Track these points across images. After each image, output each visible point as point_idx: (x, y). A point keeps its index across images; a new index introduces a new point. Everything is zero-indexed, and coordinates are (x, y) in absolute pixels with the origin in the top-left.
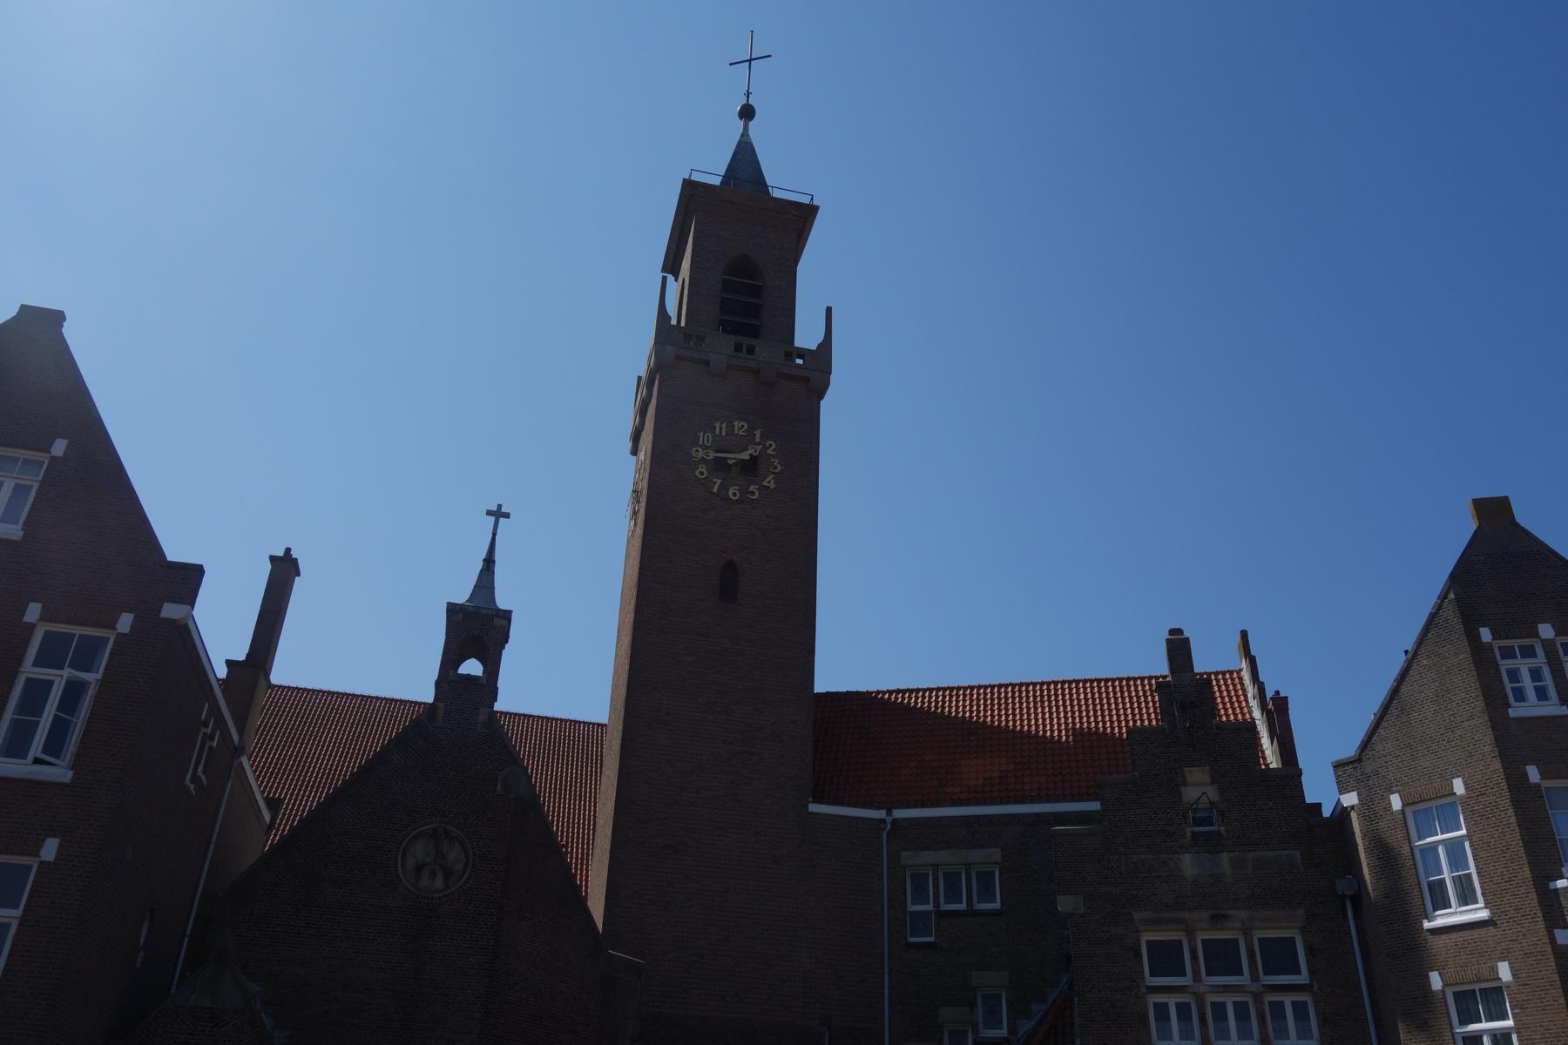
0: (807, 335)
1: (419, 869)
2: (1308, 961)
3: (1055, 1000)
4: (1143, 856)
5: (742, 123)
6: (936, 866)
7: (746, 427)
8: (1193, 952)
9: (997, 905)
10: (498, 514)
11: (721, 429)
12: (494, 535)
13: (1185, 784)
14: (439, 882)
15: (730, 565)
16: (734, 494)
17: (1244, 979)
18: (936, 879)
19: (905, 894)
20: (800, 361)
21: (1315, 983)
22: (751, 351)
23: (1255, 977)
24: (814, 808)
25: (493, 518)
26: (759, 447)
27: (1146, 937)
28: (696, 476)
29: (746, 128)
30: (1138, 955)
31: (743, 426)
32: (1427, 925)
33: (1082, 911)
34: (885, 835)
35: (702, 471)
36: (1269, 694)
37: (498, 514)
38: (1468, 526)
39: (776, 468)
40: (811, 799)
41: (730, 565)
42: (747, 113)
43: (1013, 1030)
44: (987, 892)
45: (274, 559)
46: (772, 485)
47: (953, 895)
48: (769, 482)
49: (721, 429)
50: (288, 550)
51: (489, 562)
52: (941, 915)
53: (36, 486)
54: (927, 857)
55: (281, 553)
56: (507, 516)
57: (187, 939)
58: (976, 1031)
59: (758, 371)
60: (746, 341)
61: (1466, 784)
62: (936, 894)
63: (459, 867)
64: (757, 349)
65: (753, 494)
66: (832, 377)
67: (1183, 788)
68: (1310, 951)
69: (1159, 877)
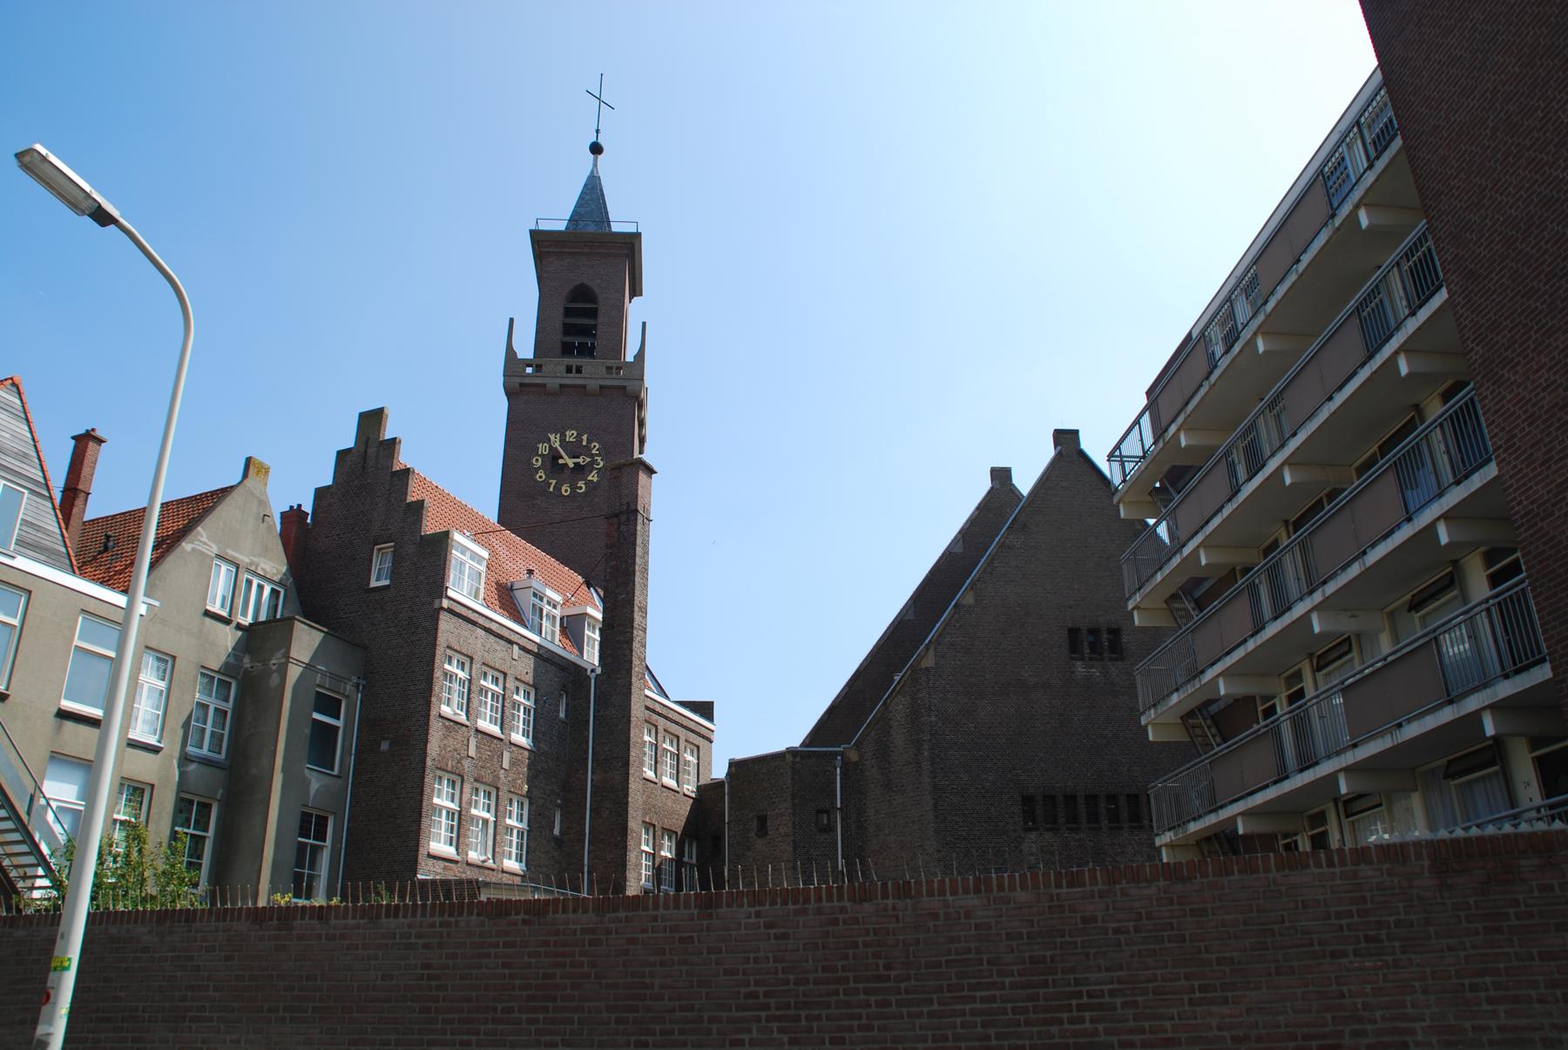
5: (112, 227)
16: (566, 491)
20: (529, 370)
22: (579, 370)
26: (588, 460)
29: (595, 164)
35: (541, 476)
50: (73, 438)
65: (581, 488)
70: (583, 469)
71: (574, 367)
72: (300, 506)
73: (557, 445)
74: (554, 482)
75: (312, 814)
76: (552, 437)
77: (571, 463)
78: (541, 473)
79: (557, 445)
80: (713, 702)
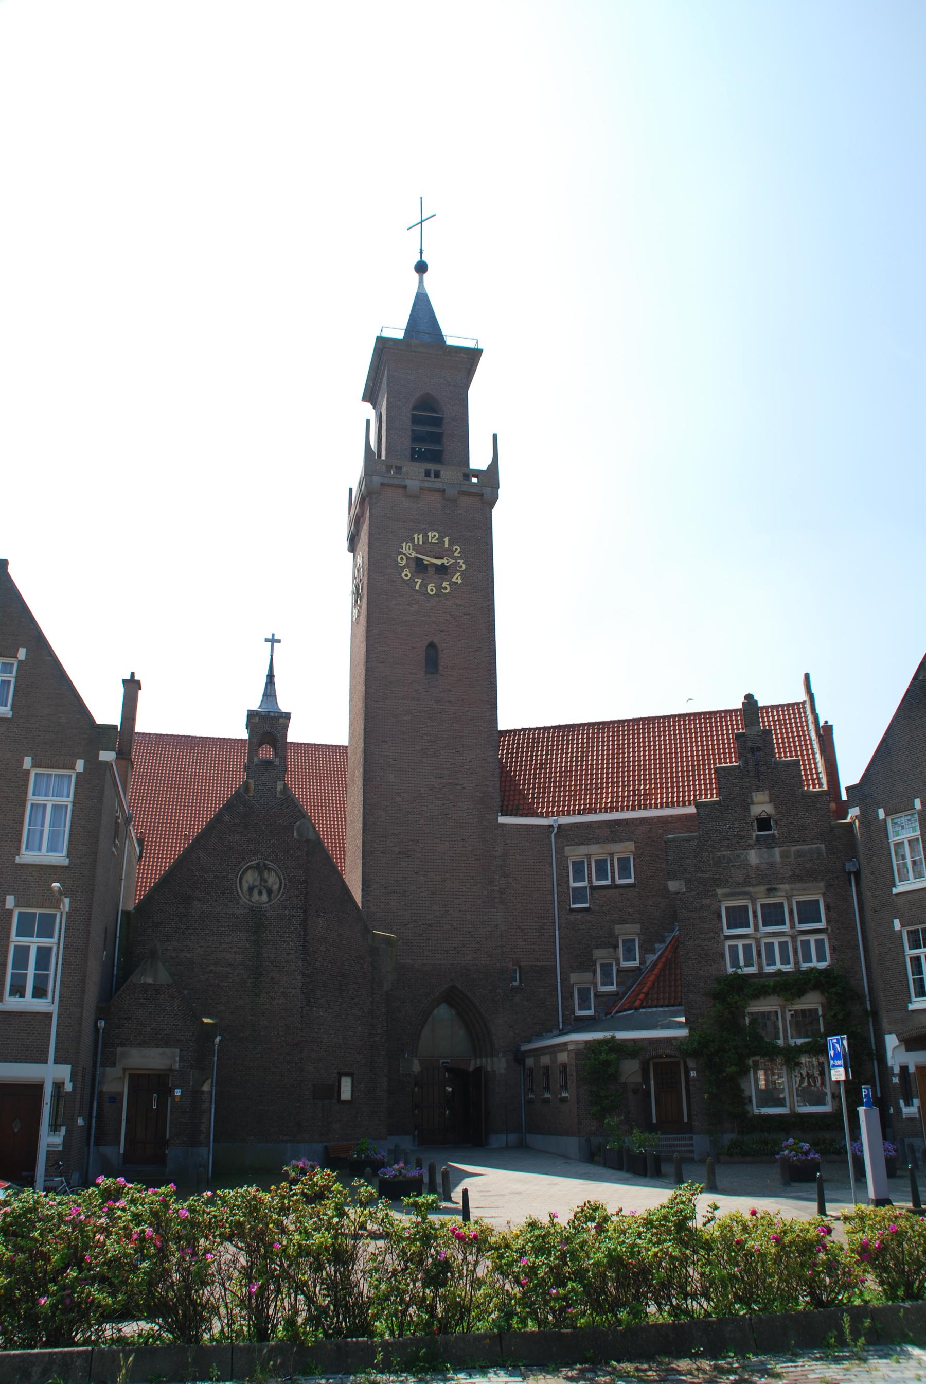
0: (479, 460)
1: (251, 889)
2: (826, 915)
3: (671, 941)
4: (724, 853)
6: (589, 856)
7: (437, 536)
8: (755, 913)
9: (631, 881)
10: (273, 641)
11: (418, 539)
12: (272, 656)
13: (753, 803)
14: (265, 897)
15: (432, 646)
16: (432, 590)
17: (785, 928)
19: (568, 876)
20: (475, 480)
21: (829, 928)
22: (437, 475)
23: (793, 926)
24: (502, 820)
25: (270, 643)
26: (452, 561)
28: (402, 578)
29: (421, 281)
30: (719, 916)
31: (435, 536)
32: (895, 891)
33: (684, 890)
34: (553, 836)
35: (406, 574)
36: (821, 723)
37: (273, 641)
39: (462, 567)
40: (500, 814)
41: (432, 646)
42: (421, 268)
43: (643, 961)
45: (125, 682)
46: (459, 581)
48: (457, 578)
49: (418, 539)
50: (133, 674)
51: (271, 677)
52: (593, 888)
53: (13, 680)
54: (583, 850)
55: (128, 677)
56: (279, 641)
57: (118, 939)
58: (618, 964)
59: (444, 491)
60: (433, 467)
63: (276, 887)
64: (442, 473)
65: (446, 589)
66: (500, 491)
67: (751, 806)
68: (828, 908)
69: (735, 865)
70: (446, 570)
71: (432, 472)
74: (420, 581)
75: (918, 930)
78: (406, 572)
80: (289, 714)
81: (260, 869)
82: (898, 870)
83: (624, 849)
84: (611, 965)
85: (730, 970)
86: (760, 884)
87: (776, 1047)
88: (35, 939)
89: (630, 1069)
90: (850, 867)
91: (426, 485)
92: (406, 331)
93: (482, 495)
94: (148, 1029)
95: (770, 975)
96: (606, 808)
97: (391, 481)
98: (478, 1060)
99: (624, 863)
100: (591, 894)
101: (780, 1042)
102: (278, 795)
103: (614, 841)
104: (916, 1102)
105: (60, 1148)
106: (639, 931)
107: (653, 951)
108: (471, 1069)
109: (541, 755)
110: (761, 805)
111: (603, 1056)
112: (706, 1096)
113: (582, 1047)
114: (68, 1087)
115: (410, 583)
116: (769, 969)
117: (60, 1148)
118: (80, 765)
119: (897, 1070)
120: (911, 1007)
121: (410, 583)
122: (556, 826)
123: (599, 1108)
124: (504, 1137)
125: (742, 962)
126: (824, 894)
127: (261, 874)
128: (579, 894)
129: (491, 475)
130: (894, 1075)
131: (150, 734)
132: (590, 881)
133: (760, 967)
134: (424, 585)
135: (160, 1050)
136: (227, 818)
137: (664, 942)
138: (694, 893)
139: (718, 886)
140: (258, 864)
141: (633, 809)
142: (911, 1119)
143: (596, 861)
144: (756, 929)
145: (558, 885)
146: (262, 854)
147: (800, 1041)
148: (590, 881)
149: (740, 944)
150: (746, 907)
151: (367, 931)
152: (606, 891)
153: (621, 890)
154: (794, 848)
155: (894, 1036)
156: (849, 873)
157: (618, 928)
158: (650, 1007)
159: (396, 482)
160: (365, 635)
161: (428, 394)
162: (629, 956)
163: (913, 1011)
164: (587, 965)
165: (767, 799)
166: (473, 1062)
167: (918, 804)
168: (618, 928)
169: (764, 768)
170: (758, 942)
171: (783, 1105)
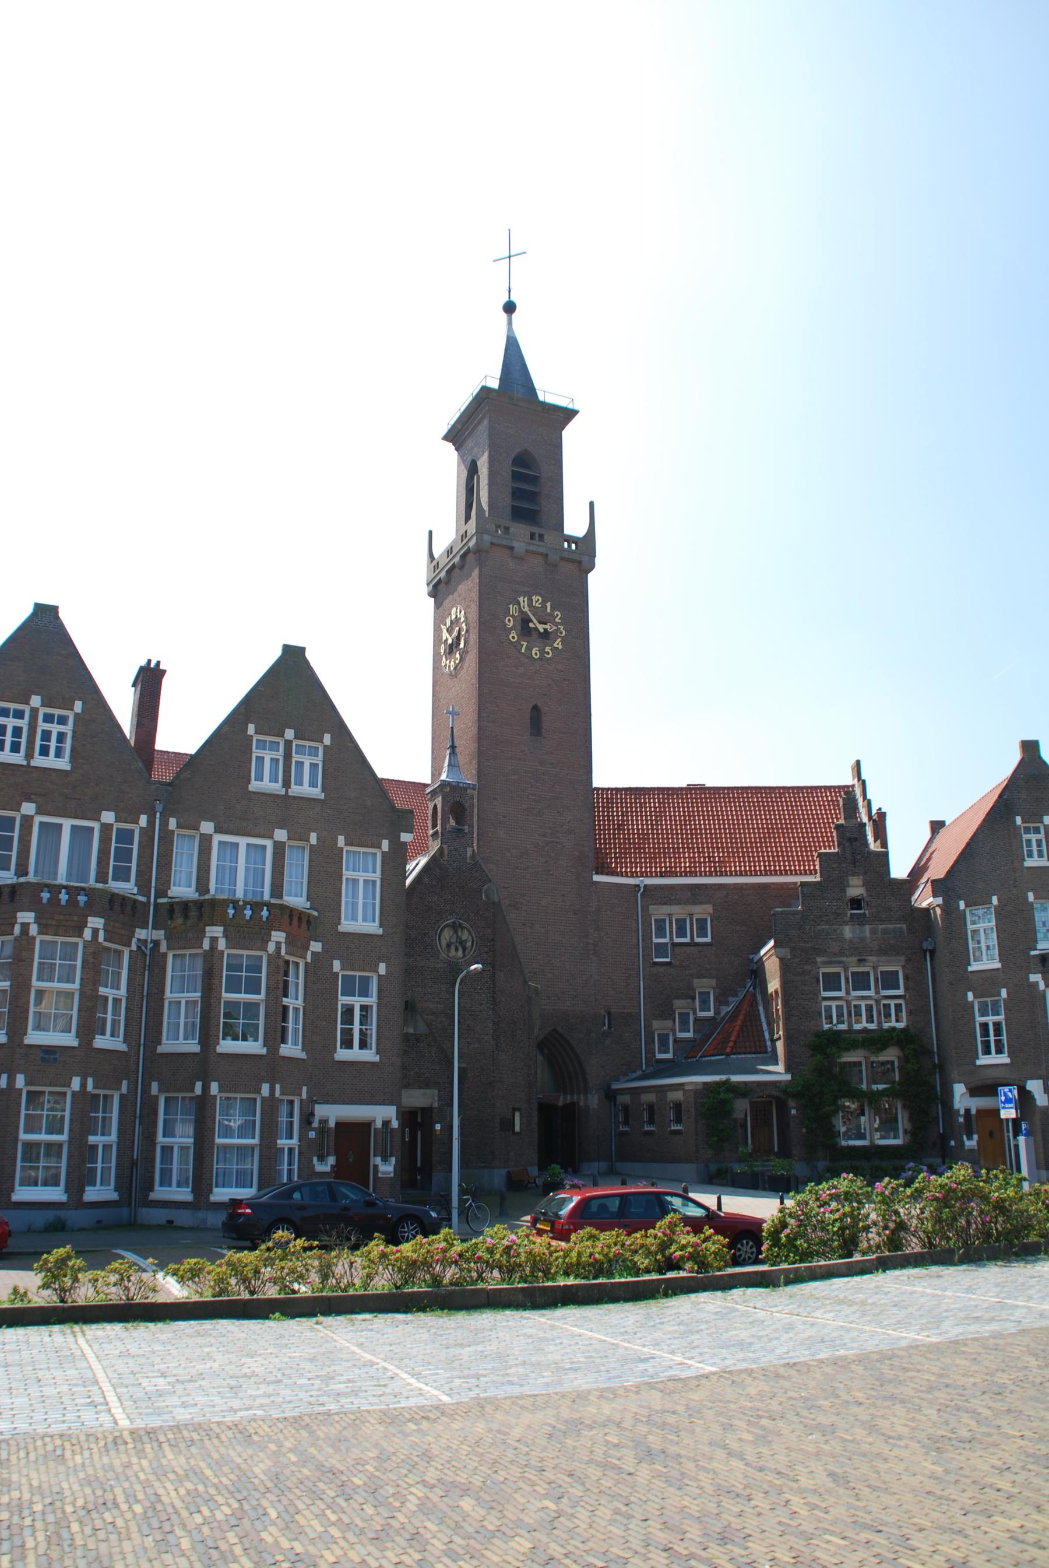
0: (574, 525)
1: (449, 946)
2: (905, 983)
6: (670, 915)
8: (847, 979)
9: (708, 939)
13: (848, 886)
14: (460, 953)
15: (535, 708)
17: (871, 993)
18: (671, 923)
22: (541, 536)
23: (877, 992)
24: (597, 878)
27: (822, 970)
29: (510, 323)
30: (818, 980)
35: (513, 636)
36: (874, 811)
38: (1014, 757)
41: (535, 708)
42: (510, 308)
43: (717, 1012)
44: (702, 932)
46: (560, 647)
47: (681, 933)
48: (558, 644)
52: (675, 945)
54: (666, 909)
58: (695, 1013)
59: (547, 555)
60: (537, 530)
61: (999, 900)
62: (671, 932)
64: (546, 537)
65: (548, 653)
66: (597, 559)
72: (158, 663)
73: (526, 609)
76: (521, 599)
77: (541, 628)
78: (513, 634)
79: (526, 609)
81: (454, 927)
82: (662, 875)
83: (702, 911)
84: (688, 1014)
85: (826, 1027)
86: (852, 955)
87: (862, 1091)
88: (356, 998)
89: (741, 1107)
90: (926, 945)
91: (532, 548)
92: (501, 380)
93: (580, 562)
94: (412, 1073)
95: (859, 1032)
96: (685, 872)
97: (499, 541)
98: (569, 1097)
99: (702, 923)
100: (673, 950)
101: (864, 1086)
102: (468, 861)
103: (694, 903)
104: (975, 1137)
105: (392, 1175)
106: (714, 985)
107: (727, 1004)
108: (561, 1104)
109: (617, 814)
110: (856, 889)
111: (722, 1096)
112: (804, 1130)
113: (700, 1087)
114: (395, 1124)
115: (517, 646)
116: (857, 1027)
117: (392, 1175)
118: (385, 845)
119: (962, 1112)
120: (978, 1062)
121: (517, 646)
122: (642, 886)
123: (715, 1139)
124: (596, 1164)
125: (835, 1021)
126: (903, 967)
127: (456, 932)
128: (661, 949)
129: (587, 543)
130: (959, 1115)
131: (168, 752)
132: (671, 938)
133: (850, 1025)
134: (529, 649)
135: (422, 1091)
136: (426, 880)
137: (737, 996)
138: (797, 960)
139: (818, 955)
140: (454, 923)
141: (711, 875)
142: (971, 1150)
143: (677, 920)
144: (848, 993)
145: (643, 940)
146: (457, 914)
147: (881, 1087)
148: (671, 938)
149: (834, 1004)
150: (839, 974)
151: (525, 982)
152: (686, 948)
153: (700, 948)
154: (881, 927)
155: (962, 1085)
156: (925, 951)
157: (696, 982)
158: (740, 1054)
159: (505, 542)
160: (475, 693)
161: (526, 450)
162: (705, 1006)
163: (980, 1066)
164: (666, 1013)
165: (861, 883)
166: (562, 1098)
167: (995, 900)
168: (696, 982)
169: (859, 857)
170: (848, 1003)
171: (865, 1138)
